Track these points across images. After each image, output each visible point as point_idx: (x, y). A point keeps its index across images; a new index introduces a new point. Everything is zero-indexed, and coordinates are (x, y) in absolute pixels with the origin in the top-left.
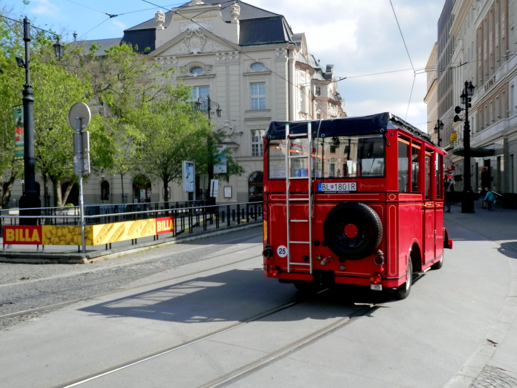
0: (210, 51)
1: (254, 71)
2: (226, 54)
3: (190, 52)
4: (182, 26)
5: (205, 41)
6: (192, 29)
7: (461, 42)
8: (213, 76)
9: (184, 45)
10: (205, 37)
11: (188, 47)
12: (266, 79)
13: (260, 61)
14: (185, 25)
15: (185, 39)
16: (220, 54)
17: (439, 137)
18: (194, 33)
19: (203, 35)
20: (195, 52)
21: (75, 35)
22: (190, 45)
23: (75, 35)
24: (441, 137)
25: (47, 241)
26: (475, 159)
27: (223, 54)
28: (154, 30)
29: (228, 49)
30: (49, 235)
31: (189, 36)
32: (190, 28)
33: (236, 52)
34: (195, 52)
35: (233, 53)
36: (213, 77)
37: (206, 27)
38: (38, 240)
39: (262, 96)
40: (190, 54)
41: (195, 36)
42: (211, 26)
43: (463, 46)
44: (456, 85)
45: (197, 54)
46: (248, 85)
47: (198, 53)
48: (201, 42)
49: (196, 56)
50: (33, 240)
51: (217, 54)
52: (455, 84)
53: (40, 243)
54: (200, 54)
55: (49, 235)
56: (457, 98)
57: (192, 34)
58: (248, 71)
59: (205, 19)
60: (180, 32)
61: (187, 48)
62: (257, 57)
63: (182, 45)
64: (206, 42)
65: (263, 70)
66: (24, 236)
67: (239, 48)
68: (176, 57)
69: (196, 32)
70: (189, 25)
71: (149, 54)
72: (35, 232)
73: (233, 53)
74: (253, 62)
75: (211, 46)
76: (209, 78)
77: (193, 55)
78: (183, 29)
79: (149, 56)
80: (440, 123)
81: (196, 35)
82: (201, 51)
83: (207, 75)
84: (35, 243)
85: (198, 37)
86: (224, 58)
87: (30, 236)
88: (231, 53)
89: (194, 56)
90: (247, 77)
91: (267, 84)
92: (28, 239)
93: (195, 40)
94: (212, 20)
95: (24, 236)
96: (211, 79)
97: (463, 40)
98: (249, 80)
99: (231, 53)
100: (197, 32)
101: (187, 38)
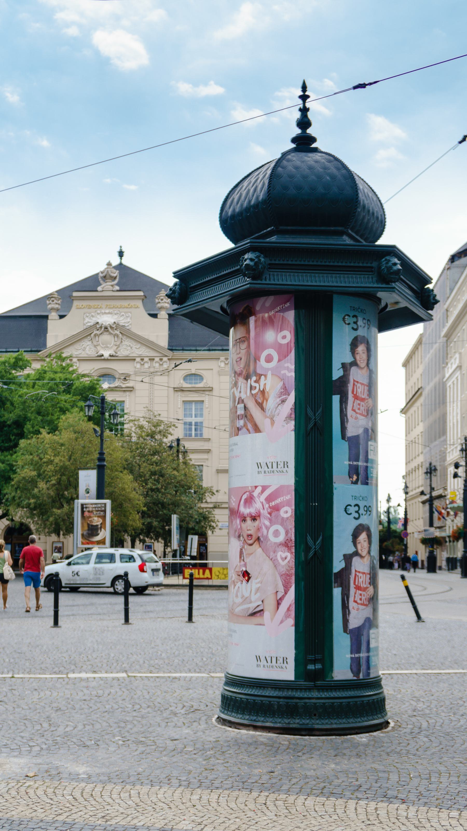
0: (127, 354)
1: (189, 386)
2: (150, 359)
3: (99, 354)
4: (87, 317)
5: (120, 340)
6: (104, 323)
7: (457, 356)
8: (131, 389)
9: (89, 343)
10: (120, 335)
11: (95, 346)
12: (205, 398)
13: (199, 372)
14: (93, 316)
15: (92, 335)
16: (142, 360)
17: (431, 485)
18: (106, 328)
19: (118, 332)
20: (106, 354)
21: (121, 254)
22: (99, 345)
23: (121, 254)
24: (433, 486)
25: (216, 577)
26: (428, 288)
27: (146, 359)
28: (46, 317)
29: (152, 354)
30: (218, 574)
31: (98, 332)
32: (100, 321)
33: (165, 359)
34: (106, 354)
35: (161, 360)
36: (131, 391)
37: (122, 321)
38: (209, 577)
39: (199, 419)
40: (98, 356)
41: (108, 333)
42: (129, 320)
43: (460, 362)
44: (451, 409)
45: (109, 358)
46: (180, 404)
47: (110, 356)
48: (115, 341)
49: (108, 360)
50: (205, 576)
51: (138, 359)
52: (450, 407)
53: (211, 578)
54: (113, 359)
55: (218, 574)
56: (452, 426)
57: (103, 328)
58: (180, 386)
59: (121, 310)
60: (84, 325)
61: (93, 348)
62: (193, 367)
63: (86, 343)
64: (122, 342)
65: (201, 385)
66: (199, 574)
67: (170, 353)
68: (78, 360)
69: (109, 328)
70: (98, 316)
71: (39, 353)
72: (207, 571)
73: (161, 360)
74: (189, 372)
75: (129, 348)
76: (124, 391)
77: (103, 358)
78: (92, 321)
79: (38, 356)
80: (433, 468)
81: (108, 331)
82: (114, 354)
83: (122, 388)
84: (207, 578)
85: (111, 334)
86: (146, 366)
87: (204, 573)
88: (157, 359)
89: (104, 360)
90: (179, 393)
91: (206, 404)
92: (201, 576)
93: (106, 337)
94: (131, 313)
95: (199, 574)
96: (128, 393)
97: (460, 354)
98: (181, 397)
99: (157, 359)
100: (111, 327)
101: (95, 335)
